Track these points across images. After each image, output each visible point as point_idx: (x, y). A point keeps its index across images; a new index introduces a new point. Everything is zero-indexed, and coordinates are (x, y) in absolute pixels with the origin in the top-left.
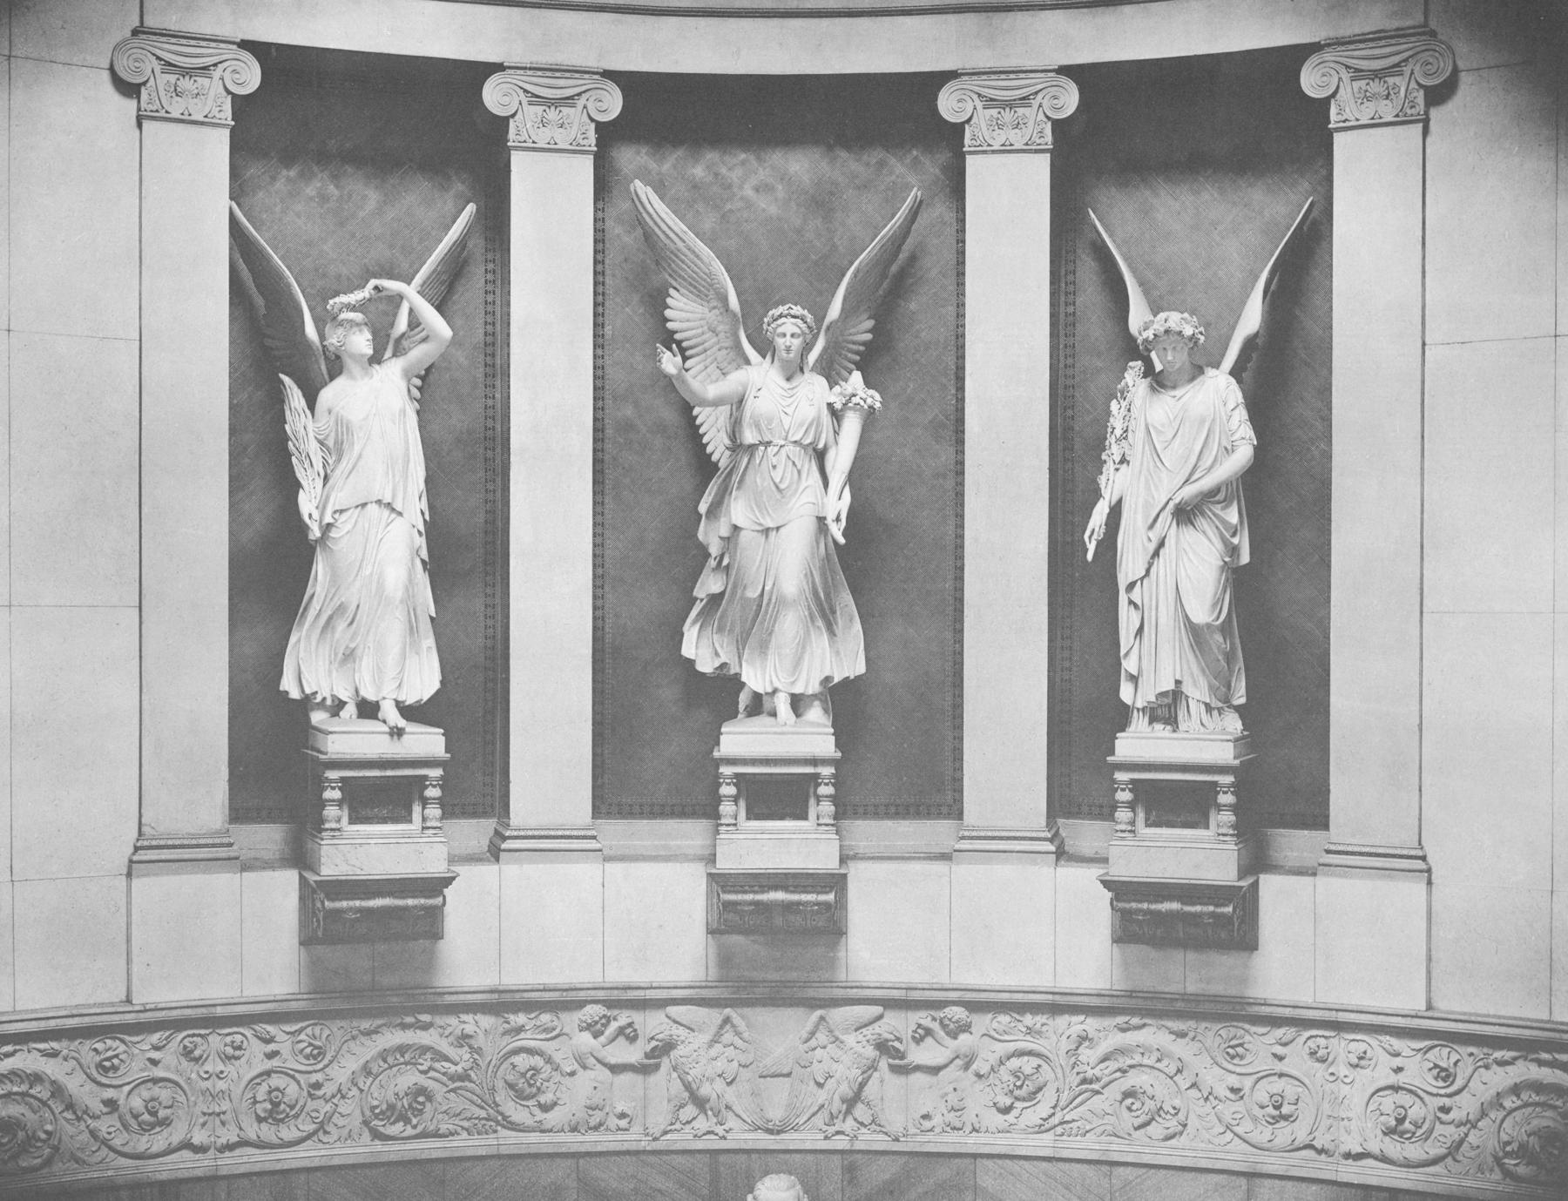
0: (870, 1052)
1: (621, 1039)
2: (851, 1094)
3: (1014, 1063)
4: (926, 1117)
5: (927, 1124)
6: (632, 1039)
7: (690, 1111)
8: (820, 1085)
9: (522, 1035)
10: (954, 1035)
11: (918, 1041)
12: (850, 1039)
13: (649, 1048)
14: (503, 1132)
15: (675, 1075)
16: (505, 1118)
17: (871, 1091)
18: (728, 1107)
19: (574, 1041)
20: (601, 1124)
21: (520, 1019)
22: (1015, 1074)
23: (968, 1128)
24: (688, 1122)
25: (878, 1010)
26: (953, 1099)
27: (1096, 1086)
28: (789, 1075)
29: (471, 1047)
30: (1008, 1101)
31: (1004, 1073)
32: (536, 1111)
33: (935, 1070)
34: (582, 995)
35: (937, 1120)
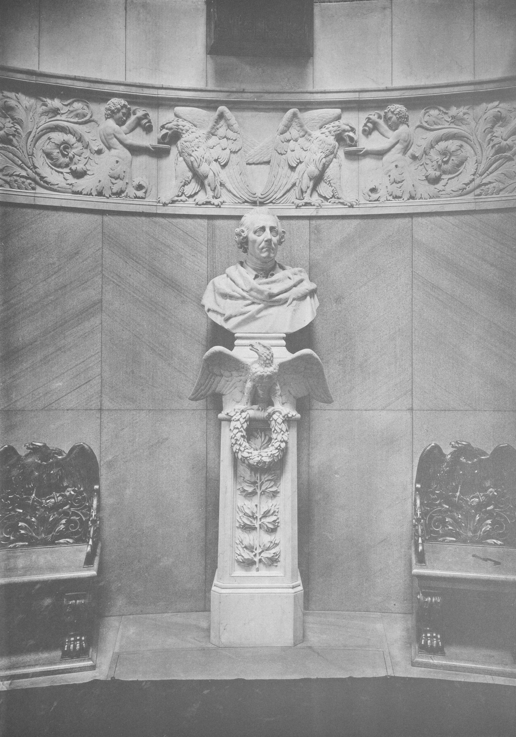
0: (331, 140)
1: (139, 130)
2: (317, 173)
3: (442, 145)
4: (373, 190)
5: (374, 196)
6: (148, 129)
7: (193, 187)
8: (293, 168)
9: (58, 117)
10: (394, 127)
11: (367, 133)
12: (316, 133)
13: (160, 135)
14: (39, 190)
15: (181, 159)
16: (42, 178)
17: (329, 173)
18: (222, 185)
19: (102, 127)
20: (122, 192)
21: (56, 103)
22: (444, 153)
23: (406, 196)
24: (191, 196)
25: (338, 111)
26: (395, 174)
27: (508, 154)
28: (268, 163)
29: (13, 118)
30: (438, 173)
31: (434, 155)
32: (69, 177)
33: (380, 154)
34: (107, 88)
35: (382, 193)
